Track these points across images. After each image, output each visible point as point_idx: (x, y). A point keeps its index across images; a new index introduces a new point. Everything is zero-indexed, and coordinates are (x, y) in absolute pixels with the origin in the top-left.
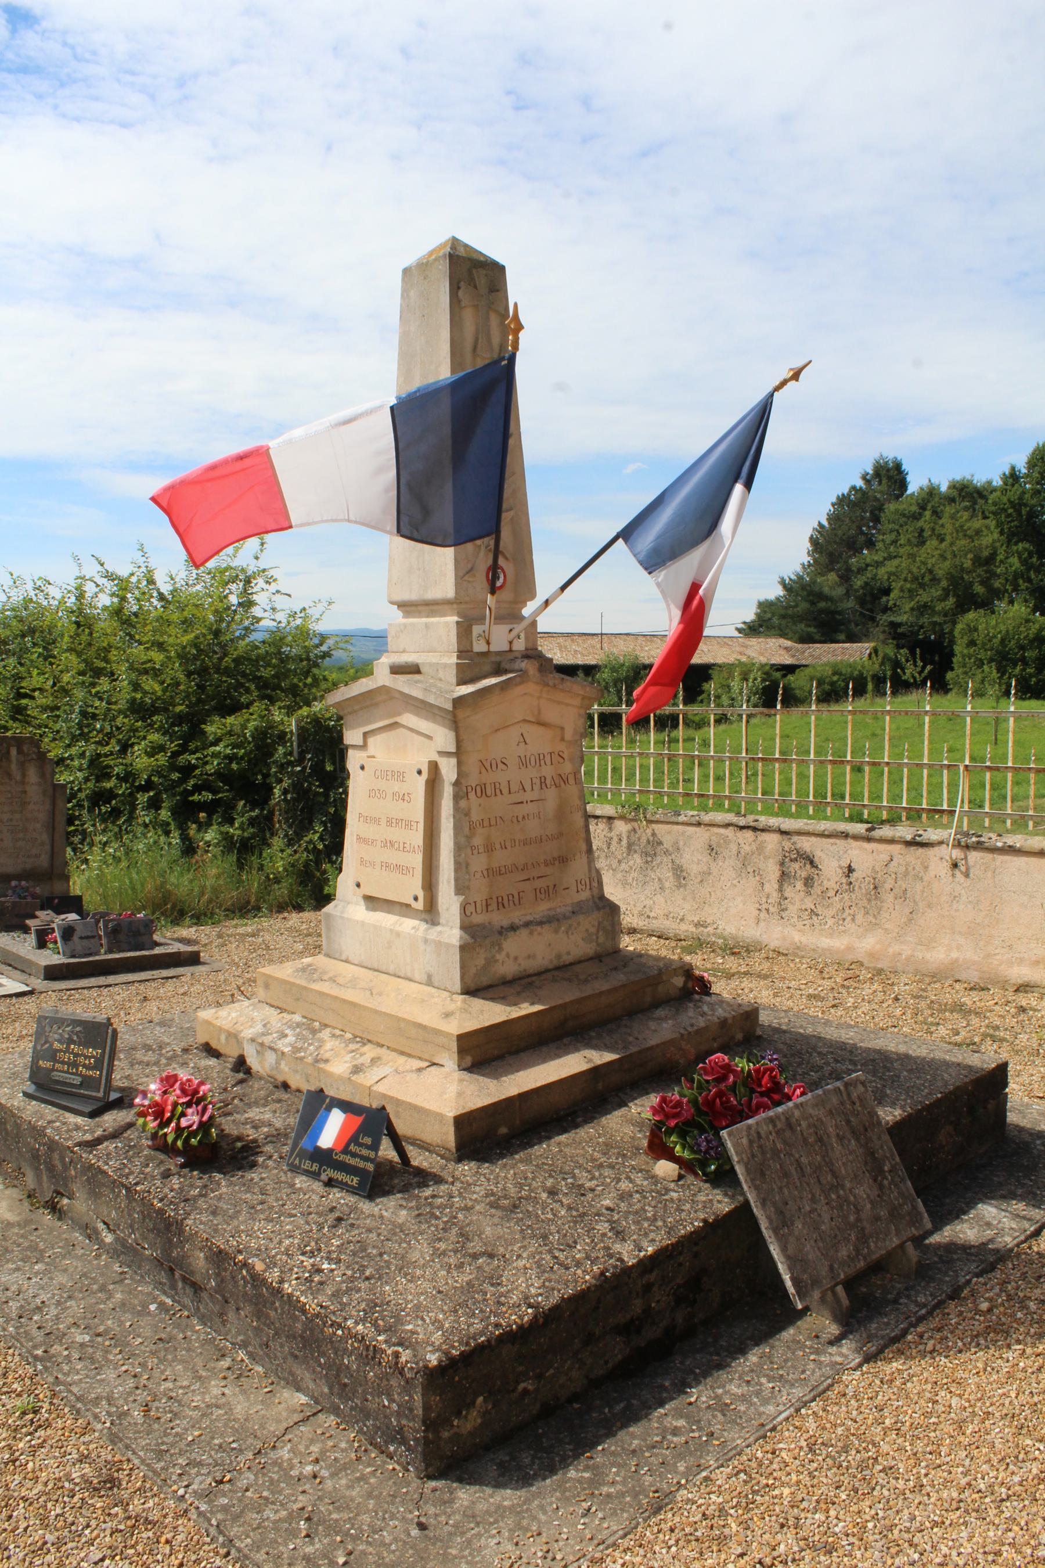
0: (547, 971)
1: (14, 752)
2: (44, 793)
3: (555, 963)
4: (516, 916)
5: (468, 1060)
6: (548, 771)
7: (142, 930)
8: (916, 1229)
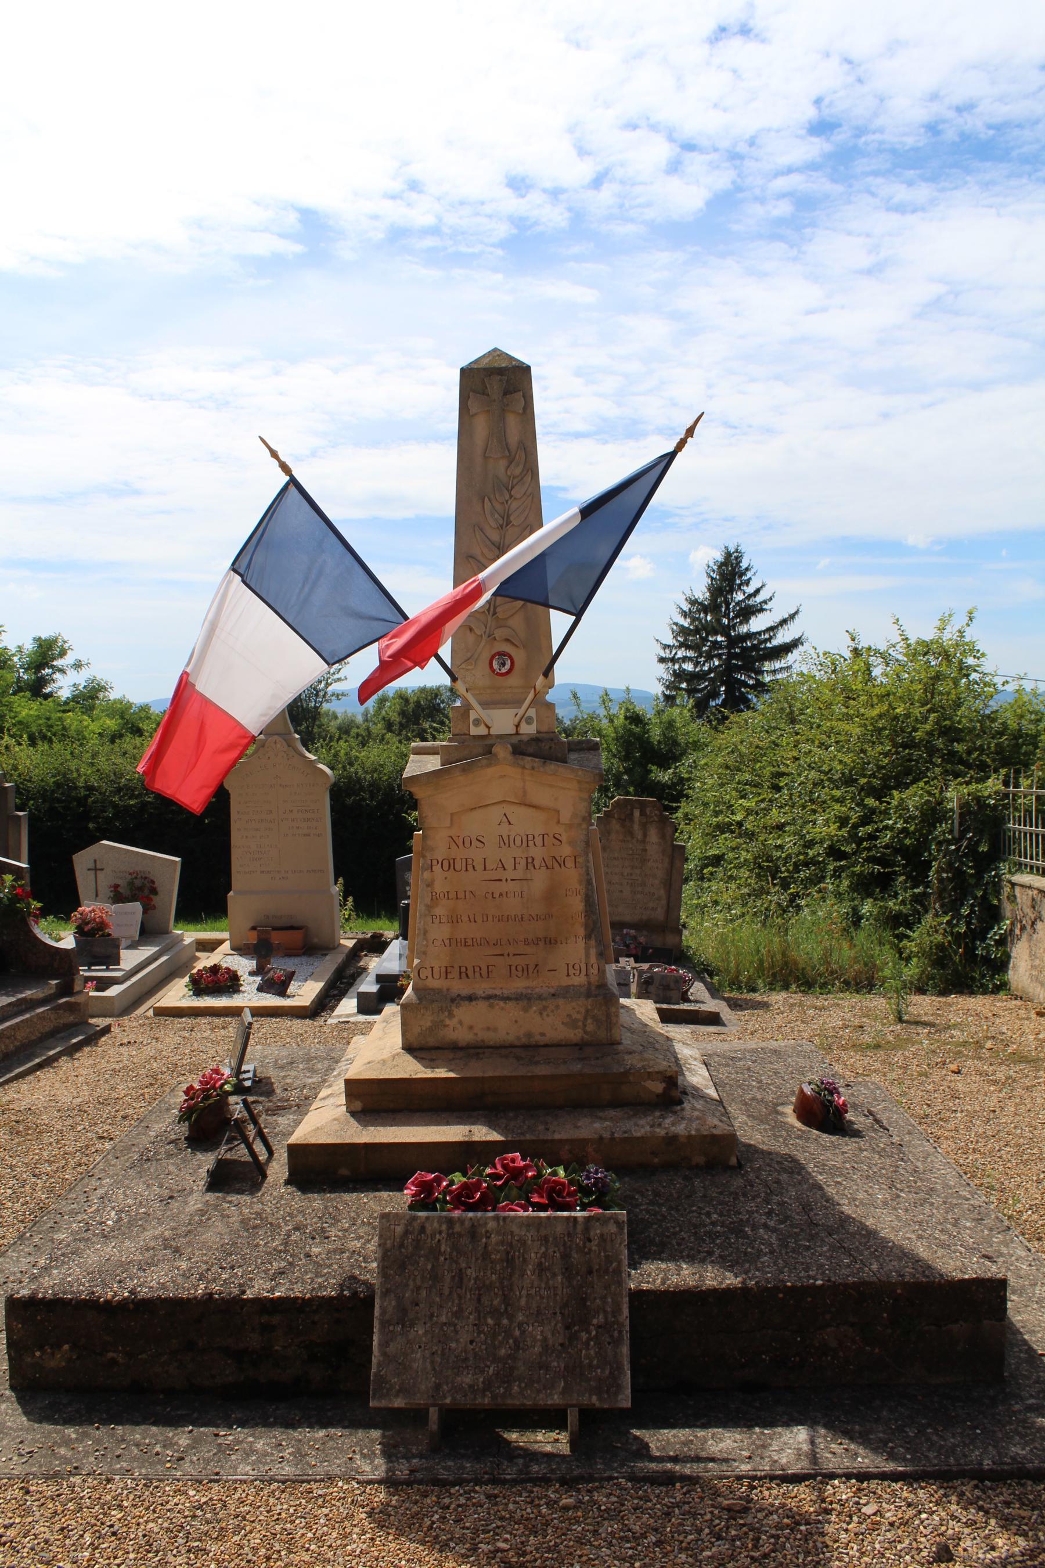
0: (512, 1046)
1: (637, 813)
3: (524, 1040)
4: (481, 988)
5: (358, 1105)
6: (537, 852)
7: (672, 985)
8: (600, 1399)
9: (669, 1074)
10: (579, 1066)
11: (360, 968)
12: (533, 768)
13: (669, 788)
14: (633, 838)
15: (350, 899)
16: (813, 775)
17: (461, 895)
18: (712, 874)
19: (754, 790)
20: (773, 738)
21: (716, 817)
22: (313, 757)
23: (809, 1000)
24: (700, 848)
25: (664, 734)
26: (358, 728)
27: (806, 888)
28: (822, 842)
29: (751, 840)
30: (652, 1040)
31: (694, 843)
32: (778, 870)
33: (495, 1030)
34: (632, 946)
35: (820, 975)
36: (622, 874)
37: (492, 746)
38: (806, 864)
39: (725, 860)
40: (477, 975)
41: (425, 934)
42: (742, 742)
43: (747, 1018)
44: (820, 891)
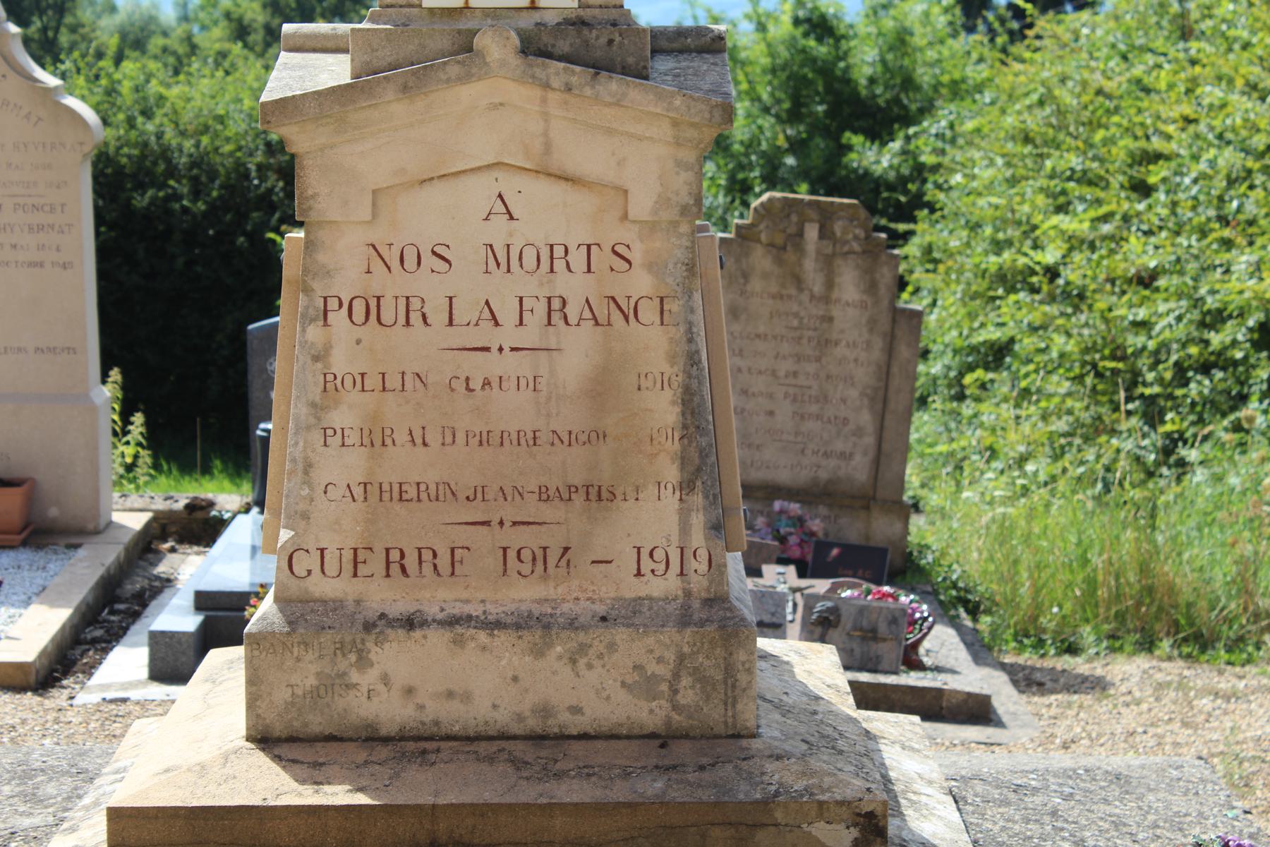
0: (504, 736)
1: (812, 232)
2: (872, 324)
3: (533, 724)
4: (436, 598)
6: (574, 287)
7: (883, 628)
9: (867, 808)
10: (659, 785)
11: (158, 578)
12: (568, 89)
13: (891, 187)
14: (801, 290)
15: (138, 418)
16: (1229, 158)
17: (393, 382)
18: (983, 386)
19: (1089, 193)
20: (1138, 71)
21: (998, 253)
22: (51, 81)
23: (1201, 676)
24: (958, 325)
25: (883, 62)
26: (165, 34)
27: (1201, 421)
28: (1242, 314)
29: (1077, 309)
30: (829, 731)
31: (947, 320)
32: (1135, 379)
33: (467, 697)
34: (793, 540)
35: (1229, 621)
36: (774, 373)
37: (474, 33)
38: (1205, 368)
39: (1015, 356)
40: (427, 568)
41: (306, 473)
42: (1063, 80)
43: (1053, 711)
44: (1237, 427)
